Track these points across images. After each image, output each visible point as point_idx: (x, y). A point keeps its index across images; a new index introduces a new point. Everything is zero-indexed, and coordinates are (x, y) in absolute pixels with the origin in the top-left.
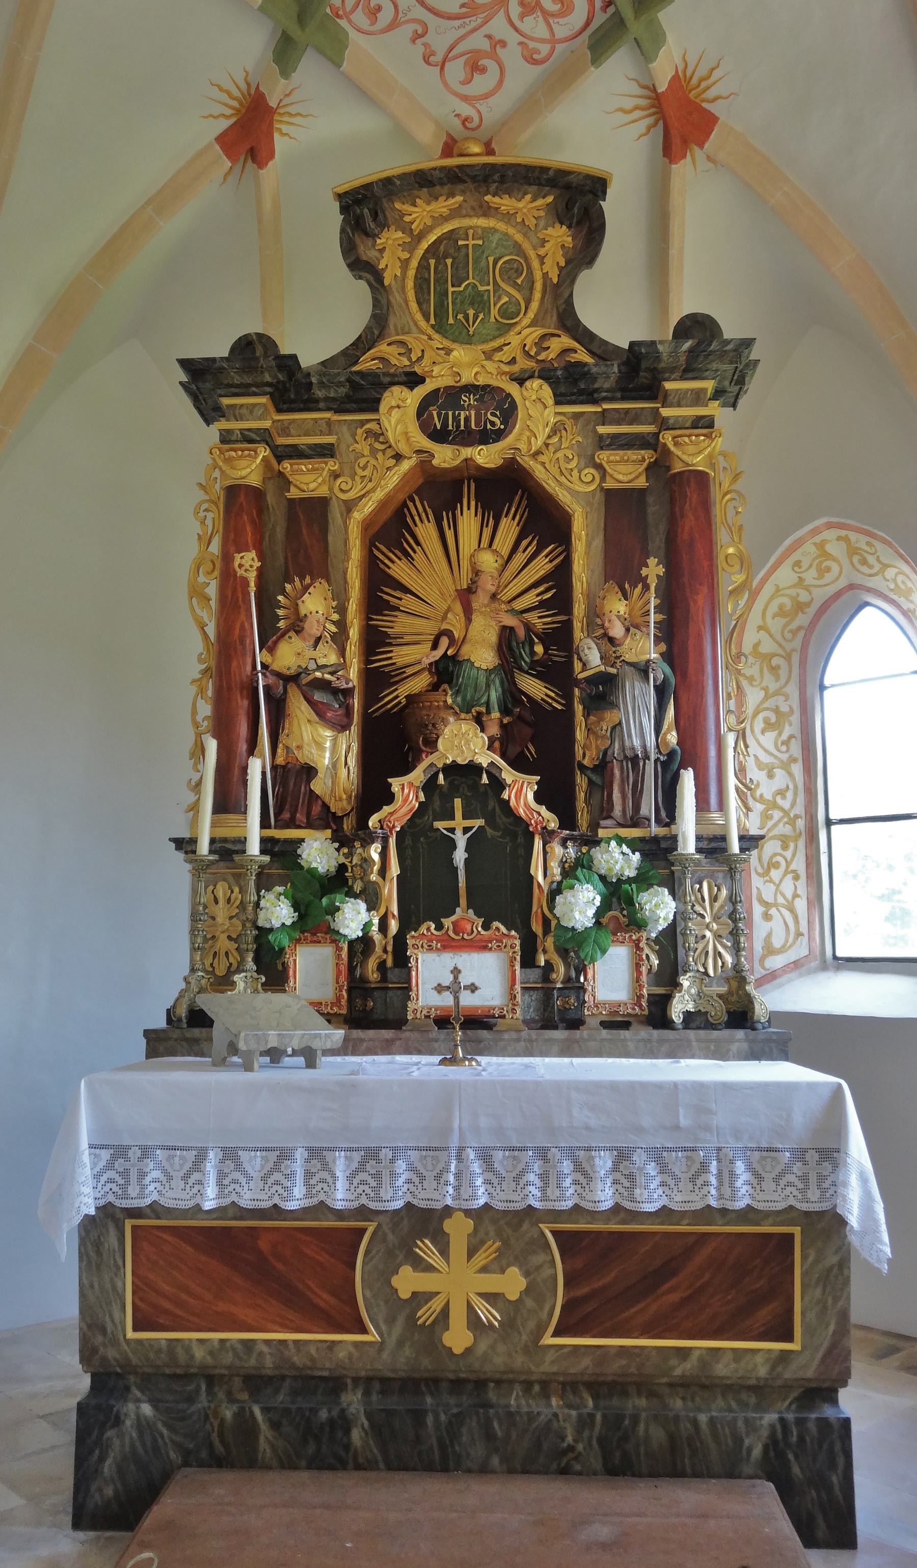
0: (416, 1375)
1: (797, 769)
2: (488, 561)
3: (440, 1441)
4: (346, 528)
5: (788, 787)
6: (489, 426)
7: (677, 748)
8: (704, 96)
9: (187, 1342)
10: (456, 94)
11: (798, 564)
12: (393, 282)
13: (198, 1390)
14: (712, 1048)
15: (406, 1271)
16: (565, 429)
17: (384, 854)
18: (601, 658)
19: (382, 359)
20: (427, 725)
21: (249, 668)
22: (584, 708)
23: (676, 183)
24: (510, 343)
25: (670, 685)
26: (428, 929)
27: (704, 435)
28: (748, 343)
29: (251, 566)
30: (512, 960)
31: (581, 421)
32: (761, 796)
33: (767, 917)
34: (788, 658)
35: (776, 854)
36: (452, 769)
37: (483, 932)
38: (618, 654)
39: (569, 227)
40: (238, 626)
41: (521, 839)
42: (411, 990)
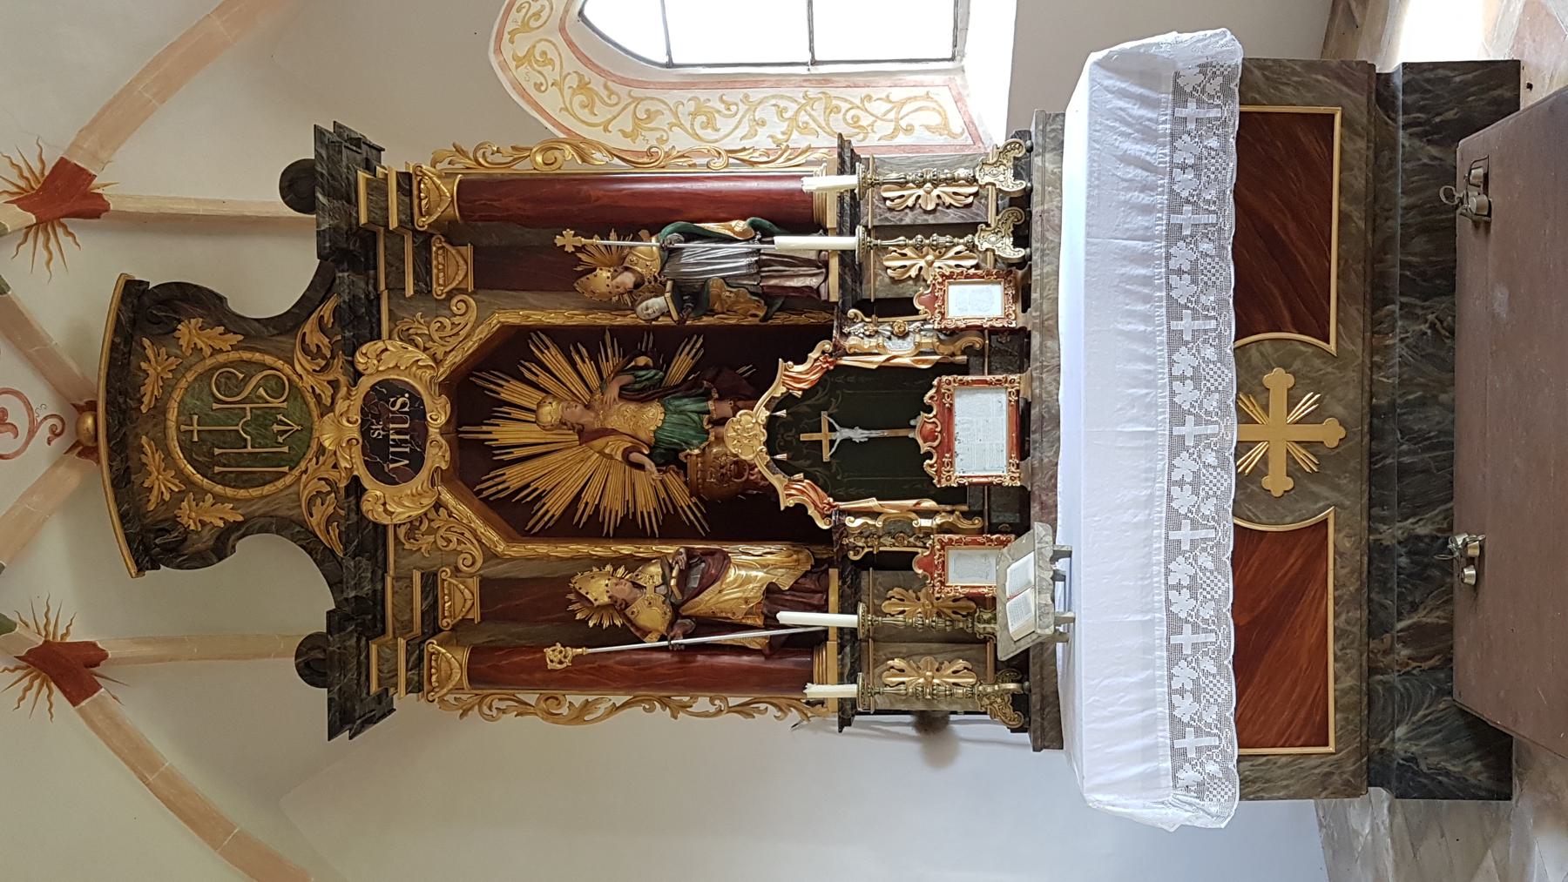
0: (1366, 472)
1: (755, 94)
2: (550, 412)
3: (1425, 450)
4: (513, 559)
5: (774, 105)
6: (406, 409)
7: (748, 220)
8: (37, 173)
9: (1337, 693)
10: (27, 443)
11: (538, 86)
12: (240, 511)
13: (1384, 683)
14: (1050, 189)
15: (1267, 482)
16: (408, 330)
17: (857, 513)
18: (656, 296)
19: (329, 521)
20: (722, 474)
21: (664, 656)
22: (705, 315)
23: (130, 207)
24: (312, 387)
25: (684, 226)
26: (932, 466)
27: (419, 183)
28: (319, 133)
29: (561, 652)
30: (962, 383)
31: (400, 314)
32: (783, 133)
33: (909, 130)
34: (638, 100)
35: (845, 119)
36: (772, 446)
37: (934, 413)
38: (652, 279)
39: (180, 322)
40: (616, 666)
41: (840, 380)
42: (992, 483)
